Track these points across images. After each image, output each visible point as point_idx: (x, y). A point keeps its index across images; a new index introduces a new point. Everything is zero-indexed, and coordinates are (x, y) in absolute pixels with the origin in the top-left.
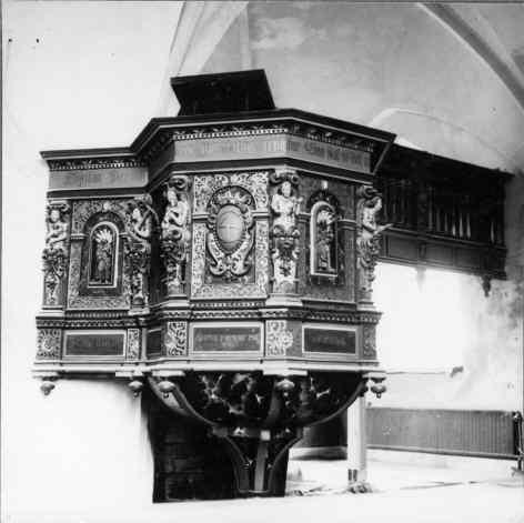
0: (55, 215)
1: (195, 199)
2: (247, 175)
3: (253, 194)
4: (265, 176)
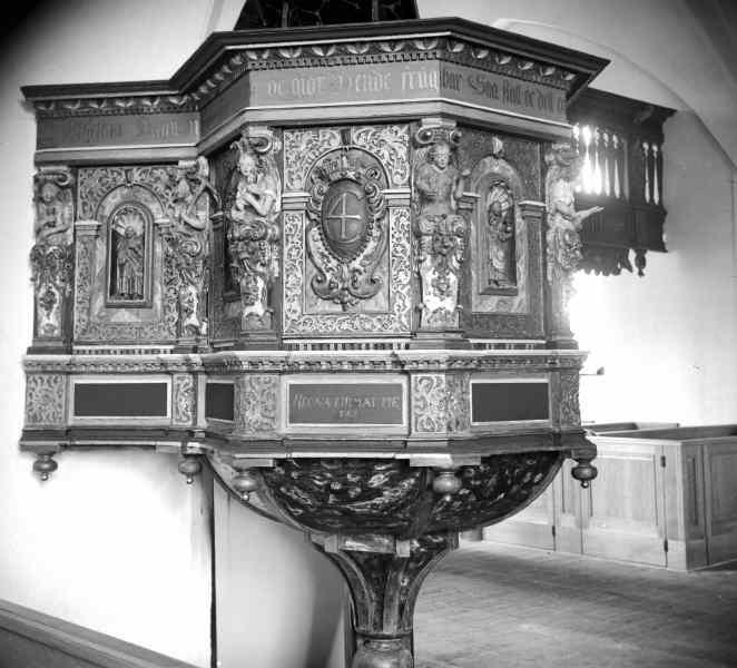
0: (49, 191)
1: (286, 171)
2: (372, 129)
3: (384, 162)
4: (402, 131)
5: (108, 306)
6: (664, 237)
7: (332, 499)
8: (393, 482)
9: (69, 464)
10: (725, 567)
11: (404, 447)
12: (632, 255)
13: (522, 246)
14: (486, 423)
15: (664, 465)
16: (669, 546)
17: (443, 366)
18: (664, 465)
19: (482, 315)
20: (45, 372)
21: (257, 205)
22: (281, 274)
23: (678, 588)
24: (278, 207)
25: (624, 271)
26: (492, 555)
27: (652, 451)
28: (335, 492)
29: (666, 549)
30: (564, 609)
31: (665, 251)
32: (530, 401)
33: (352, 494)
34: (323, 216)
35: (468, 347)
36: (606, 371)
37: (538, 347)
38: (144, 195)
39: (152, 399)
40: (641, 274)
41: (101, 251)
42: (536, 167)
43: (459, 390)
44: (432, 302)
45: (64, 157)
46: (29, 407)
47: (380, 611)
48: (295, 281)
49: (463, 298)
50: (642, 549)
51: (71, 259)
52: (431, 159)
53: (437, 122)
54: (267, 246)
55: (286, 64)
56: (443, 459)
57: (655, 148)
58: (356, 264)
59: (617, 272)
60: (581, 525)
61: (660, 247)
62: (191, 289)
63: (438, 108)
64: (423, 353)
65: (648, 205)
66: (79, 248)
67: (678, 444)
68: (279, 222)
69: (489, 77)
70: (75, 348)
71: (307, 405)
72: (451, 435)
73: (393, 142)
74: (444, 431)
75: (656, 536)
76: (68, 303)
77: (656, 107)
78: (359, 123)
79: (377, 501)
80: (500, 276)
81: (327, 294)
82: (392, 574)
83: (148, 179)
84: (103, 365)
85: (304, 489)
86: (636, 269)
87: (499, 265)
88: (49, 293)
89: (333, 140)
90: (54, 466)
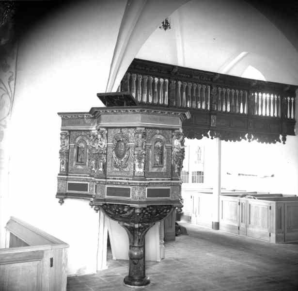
2: (127, 129)
5: (76, 164)
6: (295, 130)
7: (117, 213)
9: (67, 201)
10: (290, 243)
12: (281, 137)
13: (165, 155)
15: (270, 209)
16: (271, 235)
17: (138, 185)
18: (270, 209)
19: (152, 172)
20: (61, 180)
21: (101, 146)
22: (106, 161)
23: (268, 247)
24: (106, 146)
25: (278, 142)
26: (209, 232)
27: (267, 204)
28: (118, 212)
29: (270, 236)
30: (222, 250)
31: (294, 135)
32: (166, 193)
34: (116, 148)
35: (146, 180)
36: (275, 176)
37: (169, 180)
38: (85, 138)
40: (284, 143)
41: (75, 151)
42: (170, 136)
43: (143, 190)
44: (137, 169)
45: (67, 129)
46: (58, 188)
47: (134, 240)
49: (146, 168)
50: (264, 235)
51: (69, 153)
52: (138, 137)
54: (103, 155)
55: (108, 114)
57: (292, 99)
58: (122, 160)
59: (275, 143)
60: (247, 227)
61: (293, 134)
65: (288, 119)
66: (70, 150)
67: (275, 202)
68: (107, 150)
69: (155, 116)
70: (69, 174)
72: (140, 200)
73: (131, 133)
74: (138, 199)
75: (267, 231)
76: (67, 164)
77: (291, 86)
78: (124, 128)
79: (126, 214)
80: (158, 163)
81: (116, 167)
82: (135, 232)
83: (85, 134)
84: (75, 179)
85: (111, 211)
86: (282, 142)
88: (63, 161)
89: (118, 131)
90: (63, 202)
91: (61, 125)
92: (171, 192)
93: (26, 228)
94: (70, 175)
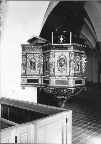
0: (24, 57)
8: (66, 91)
11: (68, 87)
14: (80, 84)
33: (62, 92)
37: (81, 76)
39: (36, 81)
44: (71, 72)
48: (56, 69)
53: (73, 53)
56: (73, 89)
62: (41, 69)
63: (73, 51)
64: (70, 78)
71: (57, 82)
79: (64, 93)
82: (64, 100)
85: (57, 92)
87: (77, 68)
91: (21, 51)
92: (82, 81)
93: (4, 123)
94: (100, 81)
